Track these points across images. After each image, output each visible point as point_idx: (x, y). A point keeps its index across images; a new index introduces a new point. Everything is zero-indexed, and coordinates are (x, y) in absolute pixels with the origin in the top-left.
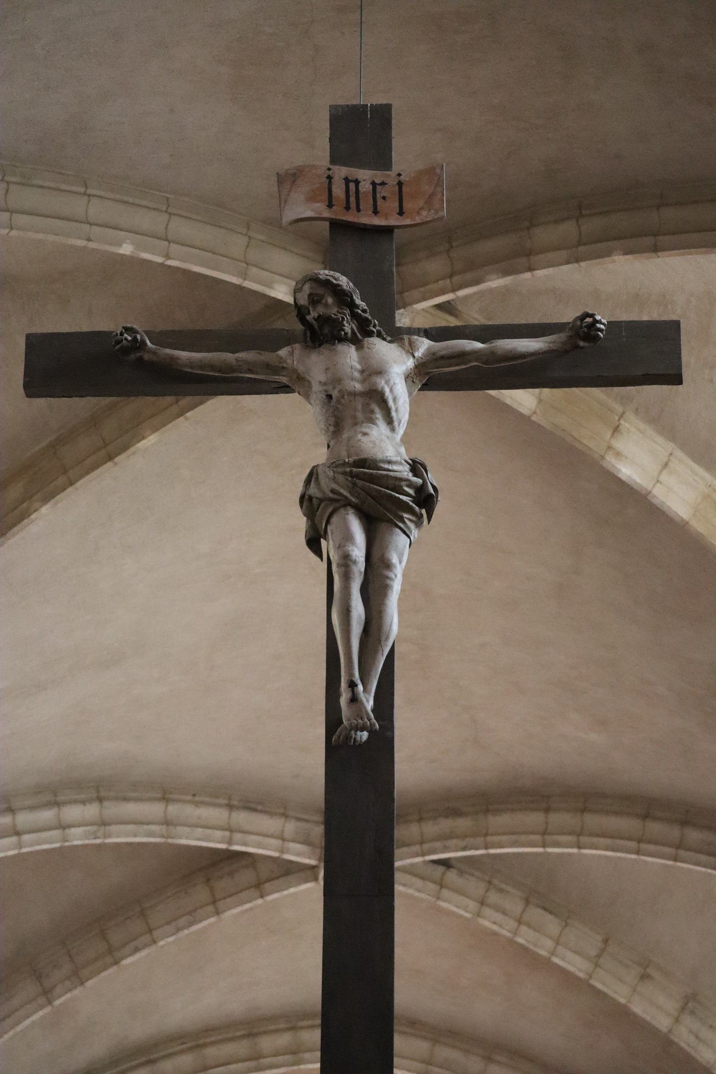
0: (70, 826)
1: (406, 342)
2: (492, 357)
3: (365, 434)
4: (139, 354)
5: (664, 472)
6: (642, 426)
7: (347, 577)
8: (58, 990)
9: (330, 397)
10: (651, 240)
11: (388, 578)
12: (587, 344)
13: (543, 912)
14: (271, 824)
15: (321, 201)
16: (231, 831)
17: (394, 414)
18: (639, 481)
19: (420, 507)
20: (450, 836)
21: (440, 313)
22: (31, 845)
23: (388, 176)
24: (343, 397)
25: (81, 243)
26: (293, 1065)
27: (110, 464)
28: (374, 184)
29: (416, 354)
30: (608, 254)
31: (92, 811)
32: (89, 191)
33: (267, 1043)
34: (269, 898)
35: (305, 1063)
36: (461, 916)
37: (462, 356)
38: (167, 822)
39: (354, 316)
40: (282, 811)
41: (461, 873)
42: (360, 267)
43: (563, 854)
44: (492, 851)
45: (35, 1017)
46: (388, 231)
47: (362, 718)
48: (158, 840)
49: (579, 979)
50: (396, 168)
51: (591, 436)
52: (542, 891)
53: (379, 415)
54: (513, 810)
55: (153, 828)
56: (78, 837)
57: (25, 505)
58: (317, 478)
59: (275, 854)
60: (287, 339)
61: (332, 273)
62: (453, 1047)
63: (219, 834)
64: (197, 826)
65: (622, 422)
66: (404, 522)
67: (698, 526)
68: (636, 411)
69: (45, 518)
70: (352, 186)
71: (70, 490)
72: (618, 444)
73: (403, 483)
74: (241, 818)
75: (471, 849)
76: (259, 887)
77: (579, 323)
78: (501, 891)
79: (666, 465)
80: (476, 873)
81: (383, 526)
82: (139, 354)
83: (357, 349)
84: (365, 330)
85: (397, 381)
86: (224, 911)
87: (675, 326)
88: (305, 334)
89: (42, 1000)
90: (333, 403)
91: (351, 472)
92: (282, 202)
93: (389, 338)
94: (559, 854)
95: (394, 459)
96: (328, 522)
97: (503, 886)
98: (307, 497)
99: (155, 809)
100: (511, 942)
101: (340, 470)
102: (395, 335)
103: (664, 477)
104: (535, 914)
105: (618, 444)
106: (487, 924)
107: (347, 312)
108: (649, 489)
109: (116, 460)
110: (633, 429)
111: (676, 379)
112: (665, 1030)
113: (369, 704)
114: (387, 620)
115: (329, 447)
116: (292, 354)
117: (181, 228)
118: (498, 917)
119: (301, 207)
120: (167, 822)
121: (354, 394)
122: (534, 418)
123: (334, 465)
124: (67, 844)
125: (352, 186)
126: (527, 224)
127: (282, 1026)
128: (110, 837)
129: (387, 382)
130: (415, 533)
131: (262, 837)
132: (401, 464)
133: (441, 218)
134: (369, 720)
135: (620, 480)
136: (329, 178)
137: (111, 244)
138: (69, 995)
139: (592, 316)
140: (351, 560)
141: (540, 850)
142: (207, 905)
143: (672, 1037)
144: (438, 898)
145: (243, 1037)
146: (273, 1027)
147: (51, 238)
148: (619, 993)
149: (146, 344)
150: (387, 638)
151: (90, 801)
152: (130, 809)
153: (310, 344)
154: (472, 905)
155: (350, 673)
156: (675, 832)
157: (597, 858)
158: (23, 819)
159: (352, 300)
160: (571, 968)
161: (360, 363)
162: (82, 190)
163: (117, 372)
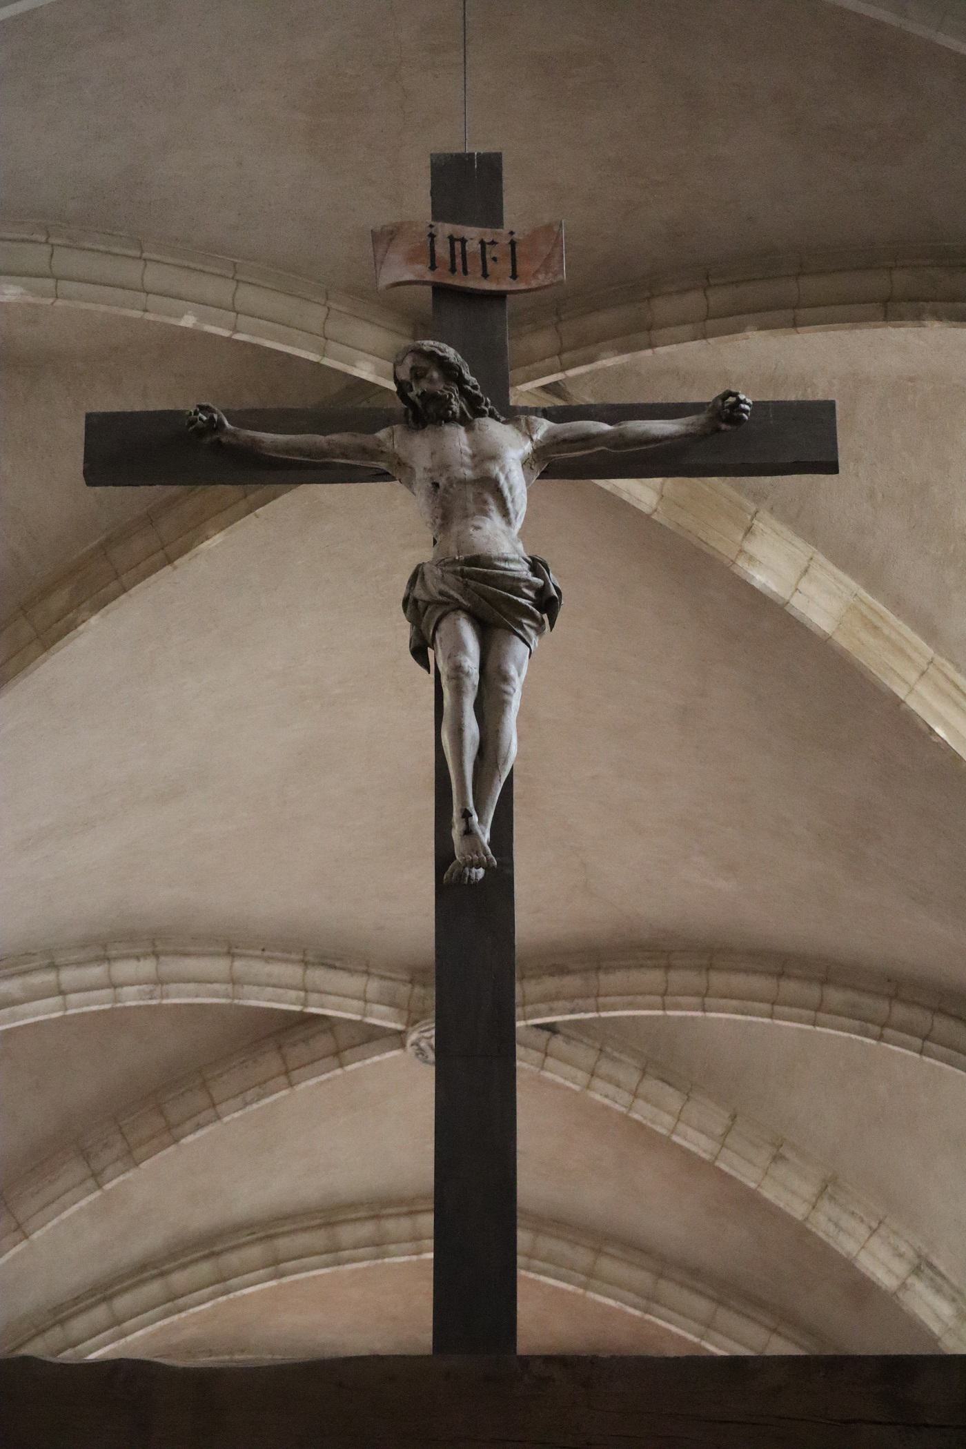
0: (122, 985)
1: (523, 422)
2: (620, 441)
3: (477, 528)
4: (215, 437)
5: (804, 579)
6: (778, 526)
7: (458, 691)
8: (109, 1172)
9: (436, 485)
10: (790, 313)
11: (506, 692)
12: (729, 427)
13: (661, 1084)
14: (353, 983)
15: (422, 262)
16: (306, 991)
17: (510, 505)
18: (775, 589)
19: (542, 612)
20: (557, 997)
21: (543, 395)
22: (77, 1007)
23: (500, 234)
24: (451, 486)
25: (137, 314)
26: (377, 1257)
27: (168, 568)
28: (482, 243)
29: (535, 437)
30: (739, 329)
31: (147, 967)
32: (145, 255)
33: (347, 1234)
34: (349, 1068)
35: (389, 1256)
36: (568, 1088)
37: (587, 440)
38: (234, 981)
39: (464, 393)
40: (364, 968)
41: (568, 1038)
42: (465, 334)
43: (685, 1018)
44: (604, 1014)
45: (83, 1203)
46: (500, 296)
47: (477, 853)
48: (223, 1001)
49: (703, 1161)
50: (507, 226)
51: (720, 539)
52: (661, 1060)
53: (493, 507)
54: (629, 968)
55: (216, 986)
56: (131, 997)
57: (71, 615)
58: (423, 578)
59: (357, 1017)
60: (387, 420)
61: (437, 344)
62: (558, 1237)
63: (293, 994)
64: (268, 985)
65: (755, 522)
66: (523, 629)
67: (842, 641)
68: (772, 510)
69: (95, 631)
70: (458, 245)
71: (123, 597)
72: (752, 547)
73: (522, 584)
74: (317, 976)
75: (581, 1011)
76: (338, 1055)
77: (720, 403)
78: (614, 1059)
79: (806, 571)
80: (585, 1040)
81: (499, 633)
82: (215, 437)
83: (467, 431)
84: (475, 409)
85: (513, 467)
86: (299, 1083)
87: (829, 407)
88: (406, 414)
89: (90, 1183)
90: (440, 492)
91: (462, 570)
92: (378, 263)
93: (503, 419)
94: (680, 1018)
95: (511, 556)
96: (436, 629)
97: (616, 1054)
98: (411, 600)
99: (218, 966)
100: (625, 1117)
101: (447, 568)
102: (510, 415)
103: (803, 585)
104: (652, 1086)
105: (752, 547)
106: (598, 1097)
107: (455, 388)
108: (787, 598)
109: (176, 563)
110: (769, 531)
111: (831, 467)
112: (800, 1218)
113: (486, 837)
114: (505, 743)
115: (435, 542)
116: (392, 436)
117: (249, 297)
118: (611, 1089)
119: (399, 269)
120: (234, 981)
121: (463, 482)
122: (654, 517)
123: (442, 563)
124: (119, 1005)
125: (458, 245)
126: (647, 294)
127: (362, 1214)
128: (167, 996)
129: (502, 469)
130: (535, 641)
131: (341, 999)
132: (519, 562)
133: (561, 282)
134: (486, 855)
135: (753, 587)
136: (432, 236)
137: (170, 315)
138: (121, 1178)
139: (735, 395)
140: (463, 672)
141: (660, 1013)
142: (278, 1075)
143: (809, 1226)
144: (542, 1068)
145: (320, 1226)
146: (353, 1216)
147: (103, 308)
148: (748, 1176)
149: (224, 425)
150: (505, 761)
151: (145, 956)
152: (192, 965)
153: (412, 423)
154: (582, 1076)
155: (464, 801)
156: (812, 992)
157: (723, 1021)
158: (69, 976)
159: (461, 375)
160: (694, 1149)
161: (471, 448)
162: (138, 253)
163: (184, 457)
